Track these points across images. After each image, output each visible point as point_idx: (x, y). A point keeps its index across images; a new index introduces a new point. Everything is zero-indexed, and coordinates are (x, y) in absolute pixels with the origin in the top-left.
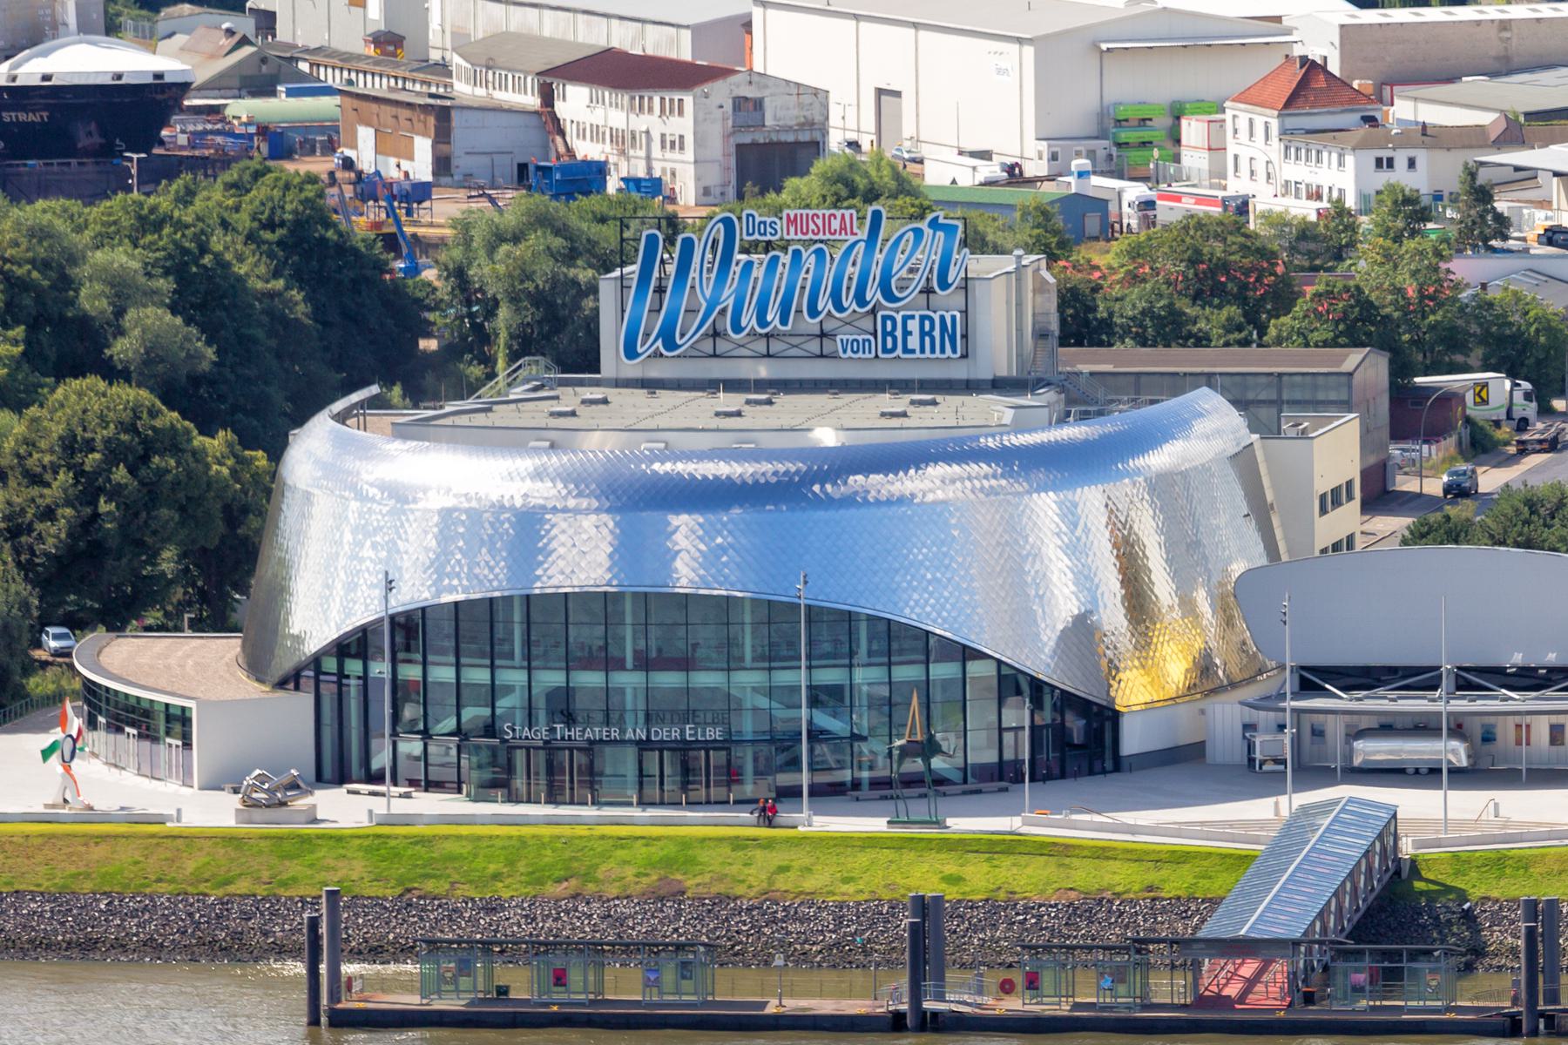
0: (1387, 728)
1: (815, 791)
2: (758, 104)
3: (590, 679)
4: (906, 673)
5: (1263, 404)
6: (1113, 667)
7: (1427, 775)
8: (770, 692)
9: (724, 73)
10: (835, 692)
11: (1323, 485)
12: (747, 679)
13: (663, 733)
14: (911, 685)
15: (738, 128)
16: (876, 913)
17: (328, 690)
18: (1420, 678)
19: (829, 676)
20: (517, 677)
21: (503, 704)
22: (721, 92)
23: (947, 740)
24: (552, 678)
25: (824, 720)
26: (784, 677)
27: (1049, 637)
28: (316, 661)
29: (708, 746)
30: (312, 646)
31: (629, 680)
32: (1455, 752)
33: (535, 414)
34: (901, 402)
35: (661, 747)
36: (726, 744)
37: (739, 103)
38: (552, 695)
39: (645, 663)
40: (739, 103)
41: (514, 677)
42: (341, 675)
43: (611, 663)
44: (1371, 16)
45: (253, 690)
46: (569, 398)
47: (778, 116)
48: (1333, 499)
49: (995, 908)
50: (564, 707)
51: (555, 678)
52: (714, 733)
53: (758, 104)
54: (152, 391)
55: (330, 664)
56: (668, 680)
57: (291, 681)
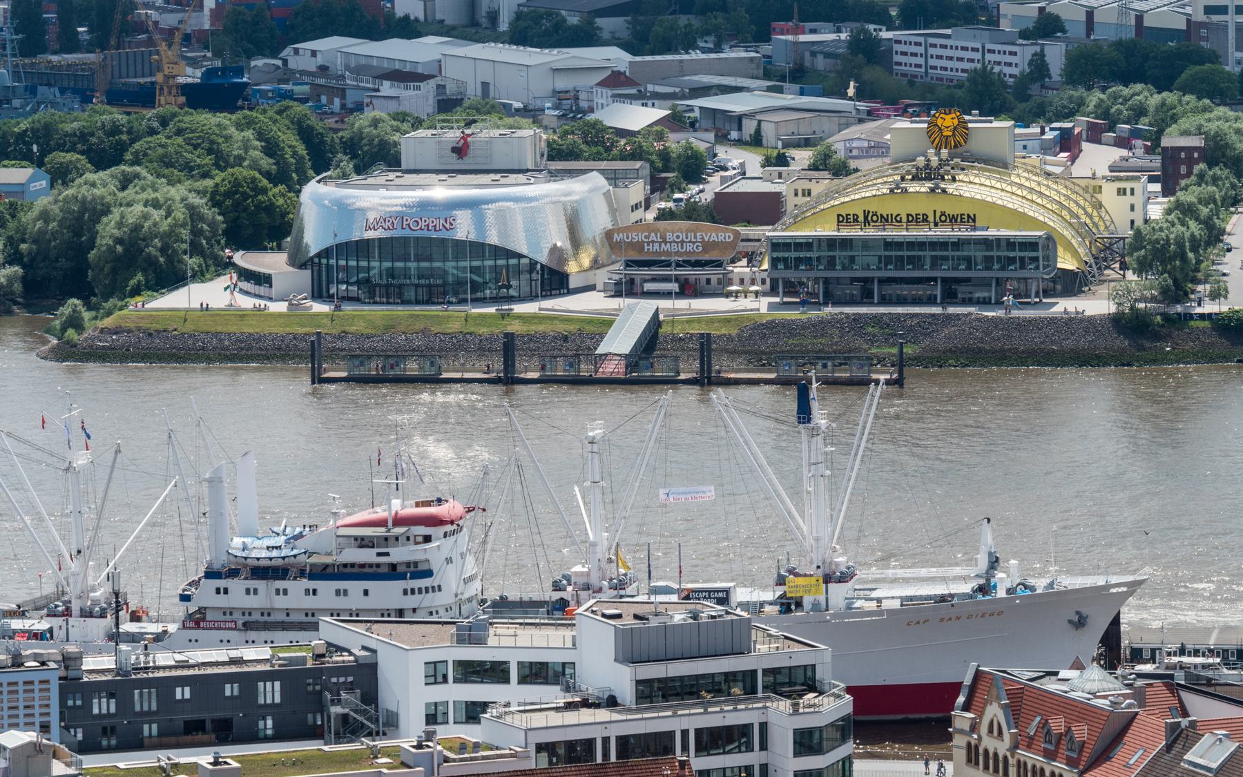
0: (654, 279)
1: (472, 300)
2: (444, 87)
3: (399, 264)
4: (501, 262)
5: (614, 178)
6: (566, 260)
7: (667, 295)
8: (457, 268)
9: (433, 77)
10: (478, 268)
11: (633, 203)
12: (450, 265)
13: (422, 282)
14: (502, 266)
15: (438, 94)
16: (492, 338)
17: (316, 268)
18: (667, 264)
19: (476, 263)
20: (376, 264)
21: (372, 273)
22: (432, 83)
23: (514, 283)
24: (387, 264)
25: (475, 278)
26: (462, 264)
27: (546, 252)
28: (312, 259)
29: (438, 286)
30: (312, 254)
31: (412, 265)
32: (674, 287)
33: (381, 180)
34: (498, 177)
35: (423, 286)
36: (444, 285)
37: (438, 86)
38: (388, 269)
39: (418, 259)
40: (438, 86)
41: (375, 264)
42: (320, 263)
43: (406, 259)
44: (639, 59)
45: (291, 269)
46: (392, 176)
47: (451, 89)
48: (636, 207)
49: (531, 338)
50: (391, 273)
51: (389, 264)
52: (439, 282)
53: (444, 87)
54: (882, 40)
55: (316, 260)
56: (424, 264)
57: (302, 266)
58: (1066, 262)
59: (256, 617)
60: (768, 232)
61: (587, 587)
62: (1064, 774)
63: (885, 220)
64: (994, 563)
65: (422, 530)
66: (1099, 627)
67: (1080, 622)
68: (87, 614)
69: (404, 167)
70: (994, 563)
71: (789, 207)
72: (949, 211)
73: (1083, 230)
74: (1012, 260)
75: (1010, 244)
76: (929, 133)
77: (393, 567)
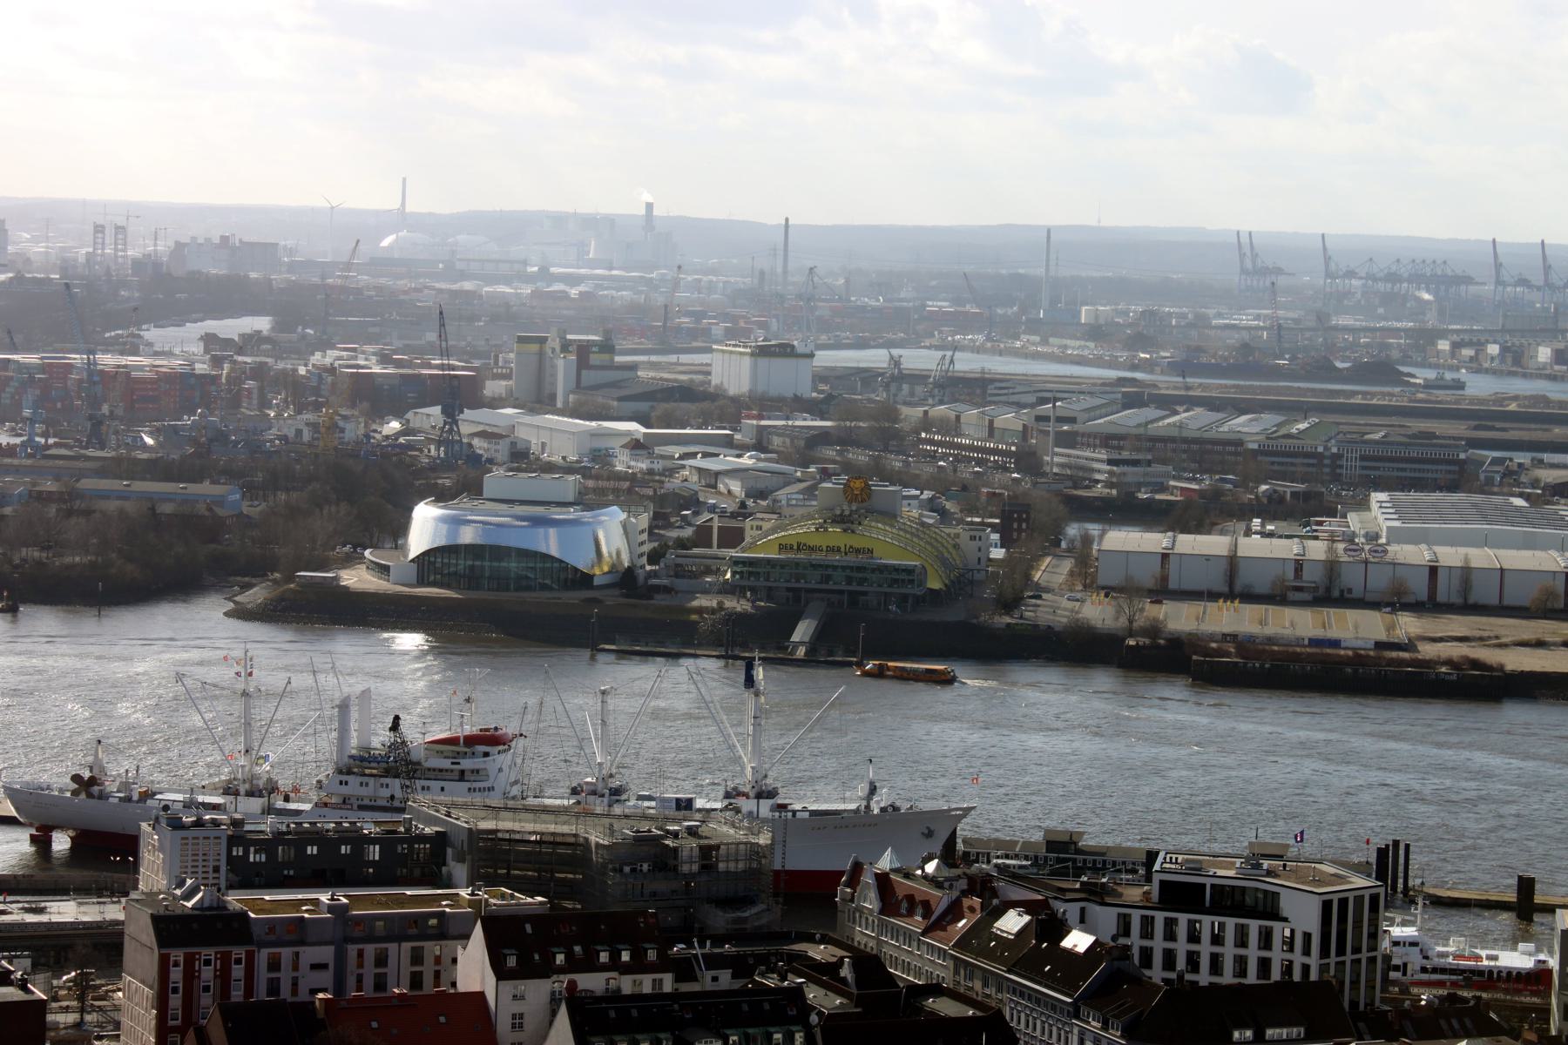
22: (508, 440)
56: (495, 564)
58: (934, 584)
59: (366, 802)
60: (733, 553)
61: (594, 793)
62: (1019, 1019)
63: (812, 549)
64: (873, 790)
65: (482, 748)
66: (943, 836)
67: (929, 834)
68: (250, 794)
69: (487, 493)
70: (873, 790)
71: (748, 539)
72: (856, 546)
73: (944, 562)
74: (896, 581)
75: (896, 569)
76: (845, 491)
77: (462, 772)
